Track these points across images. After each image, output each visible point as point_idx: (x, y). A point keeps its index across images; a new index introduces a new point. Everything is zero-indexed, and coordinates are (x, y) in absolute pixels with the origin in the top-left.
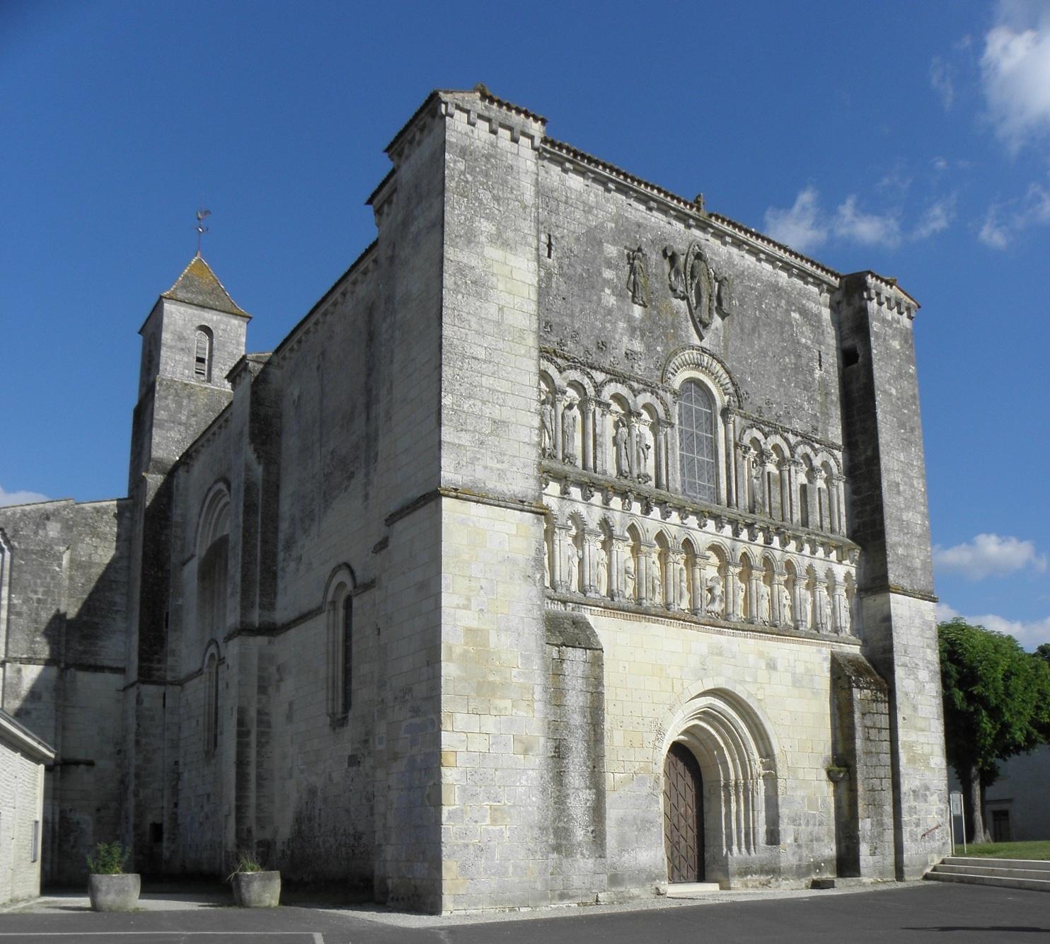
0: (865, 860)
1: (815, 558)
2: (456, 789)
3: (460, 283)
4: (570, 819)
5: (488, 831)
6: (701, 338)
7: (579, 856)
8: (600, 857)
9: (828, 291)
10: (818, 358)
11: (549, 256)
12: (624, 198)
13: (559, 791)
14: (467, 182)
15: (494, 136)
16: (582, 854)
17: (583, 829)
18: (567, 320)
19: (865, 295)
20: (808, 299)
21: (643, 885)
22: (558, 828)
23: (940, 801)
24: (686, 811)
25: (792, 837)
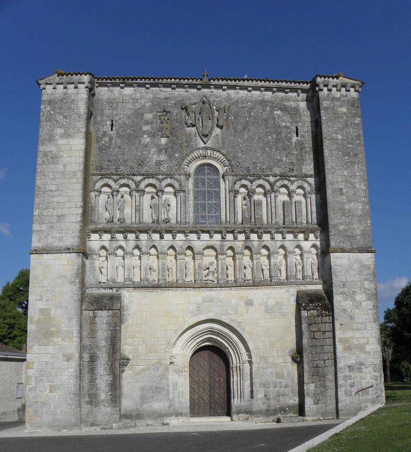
0: (309, 407)
1: (286, 241)
2: (33, 378)
3: (45, 160)
4: (98, 389)
5: (48, 396)
6: (205, 143)
7: (102, 406)
8: (115, 407)
9: (302, 92)
10: (295, 131)
11: (112, 130)
12: (158, 88)
13: (92, 377)
14: (51, 115)
15: (66, 89)
16: (104, 406)
17: (105, 394)
18: (120, 157)
19: (317, 89)
20: (288, 101)
21: (156, 419)
22: (91, 393)
23: (374, 371)
24: (220, 380)
25: (263, 395)
